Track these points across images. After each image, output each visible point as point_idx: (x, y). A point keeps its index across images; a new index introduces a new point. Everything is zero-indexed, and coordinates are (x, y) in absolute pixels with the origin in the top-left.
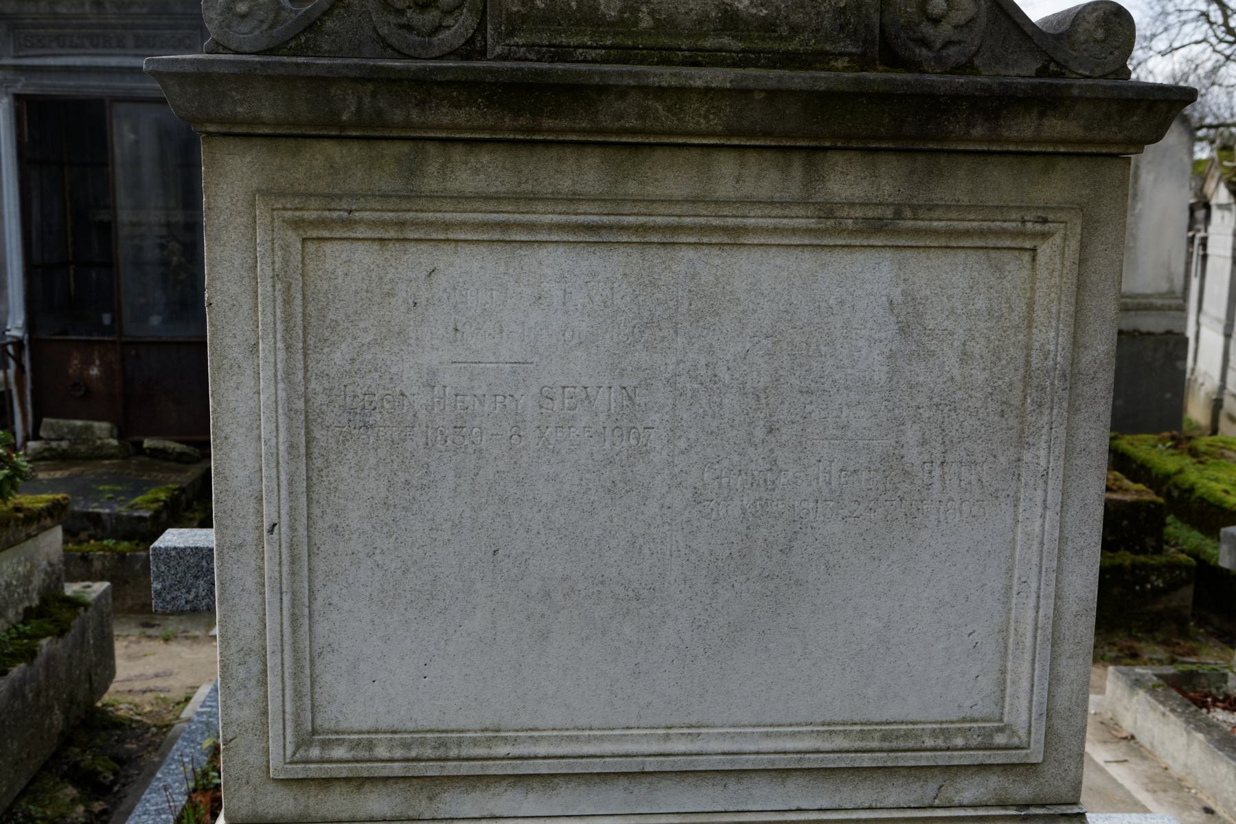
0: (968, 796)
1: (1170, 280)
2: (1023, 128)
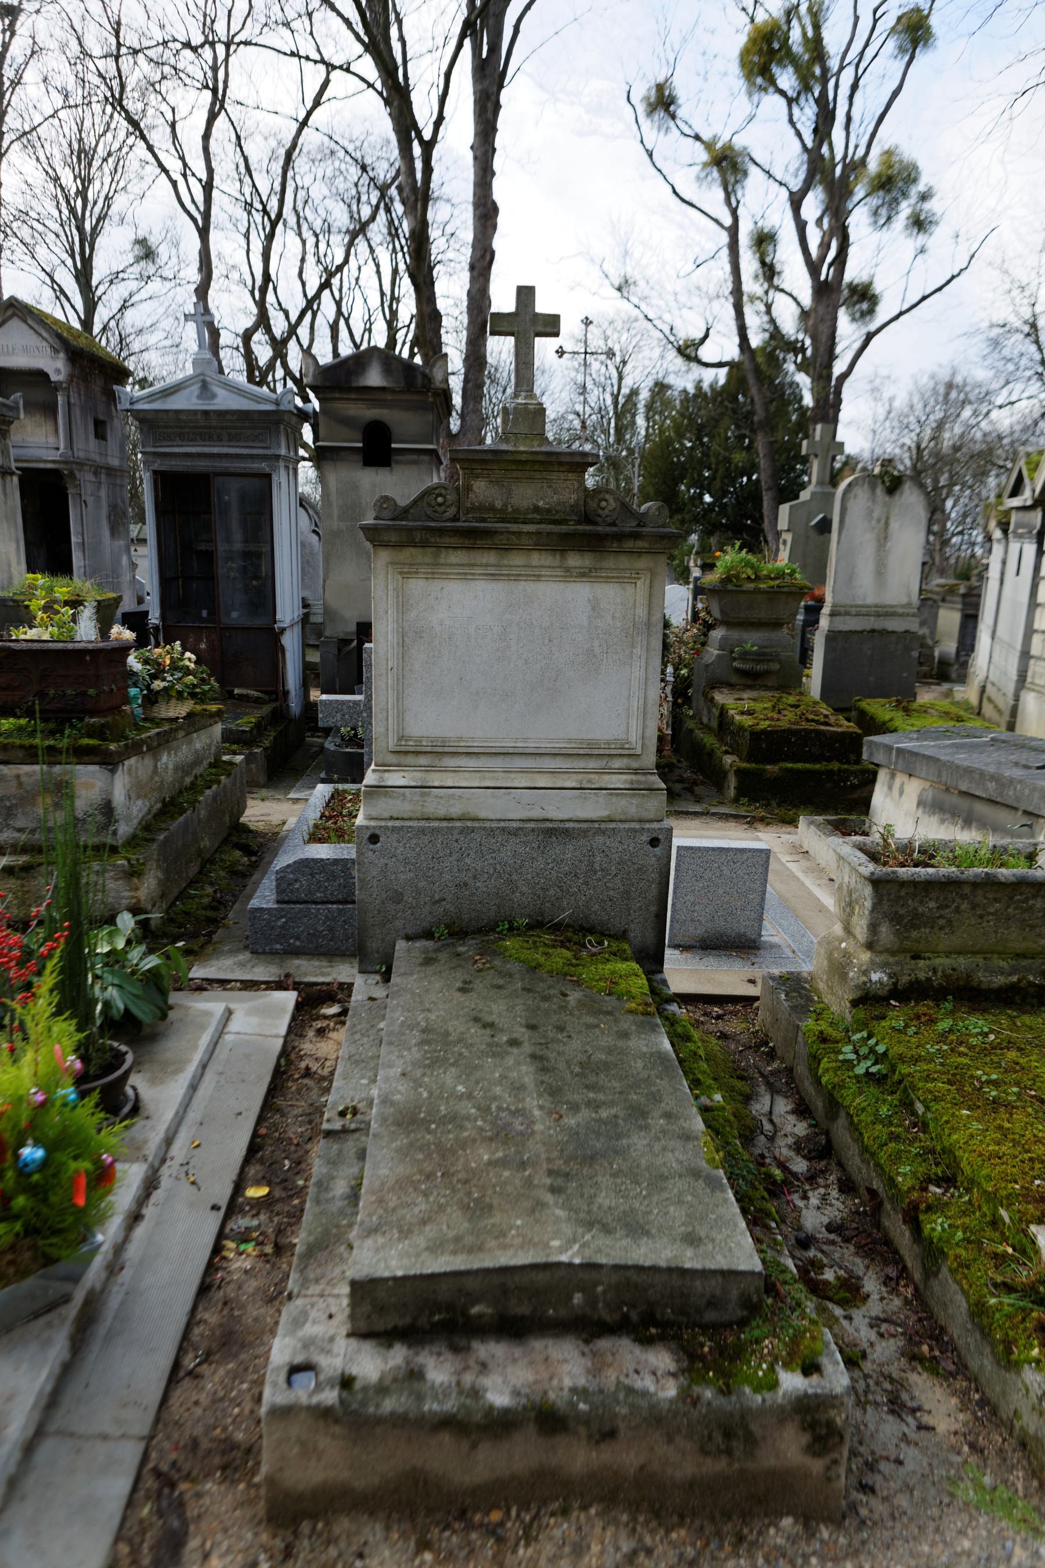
0: (616, 766)
1: (909, 595)
2: (629, 544)
